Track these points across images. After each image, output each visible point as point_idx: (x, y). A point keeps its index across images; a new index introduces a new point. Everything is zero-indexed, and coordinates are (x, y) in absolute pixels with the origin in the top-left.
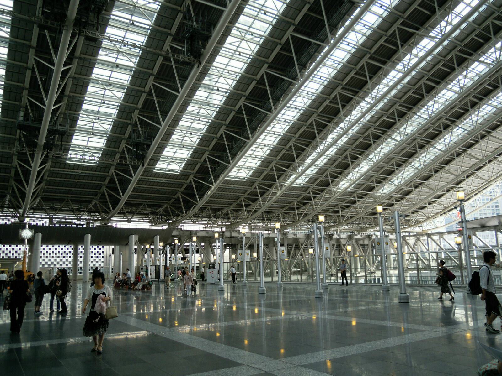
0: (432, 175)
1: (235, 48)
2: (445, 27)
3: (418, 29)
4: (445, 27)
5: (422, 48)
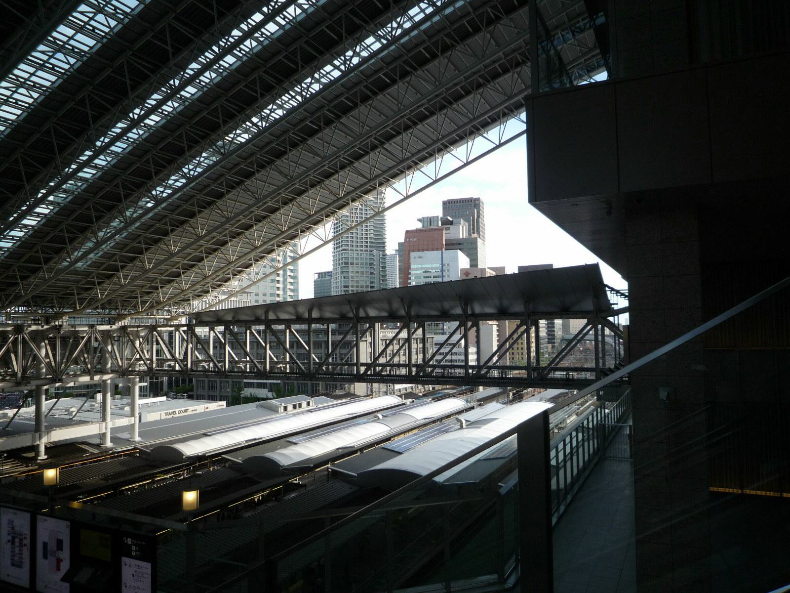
0: (323, 219)
1: (86, 19)
2: (352, 57)
3: (366, 22)
4: (352, 57)
5: (325, 73)
